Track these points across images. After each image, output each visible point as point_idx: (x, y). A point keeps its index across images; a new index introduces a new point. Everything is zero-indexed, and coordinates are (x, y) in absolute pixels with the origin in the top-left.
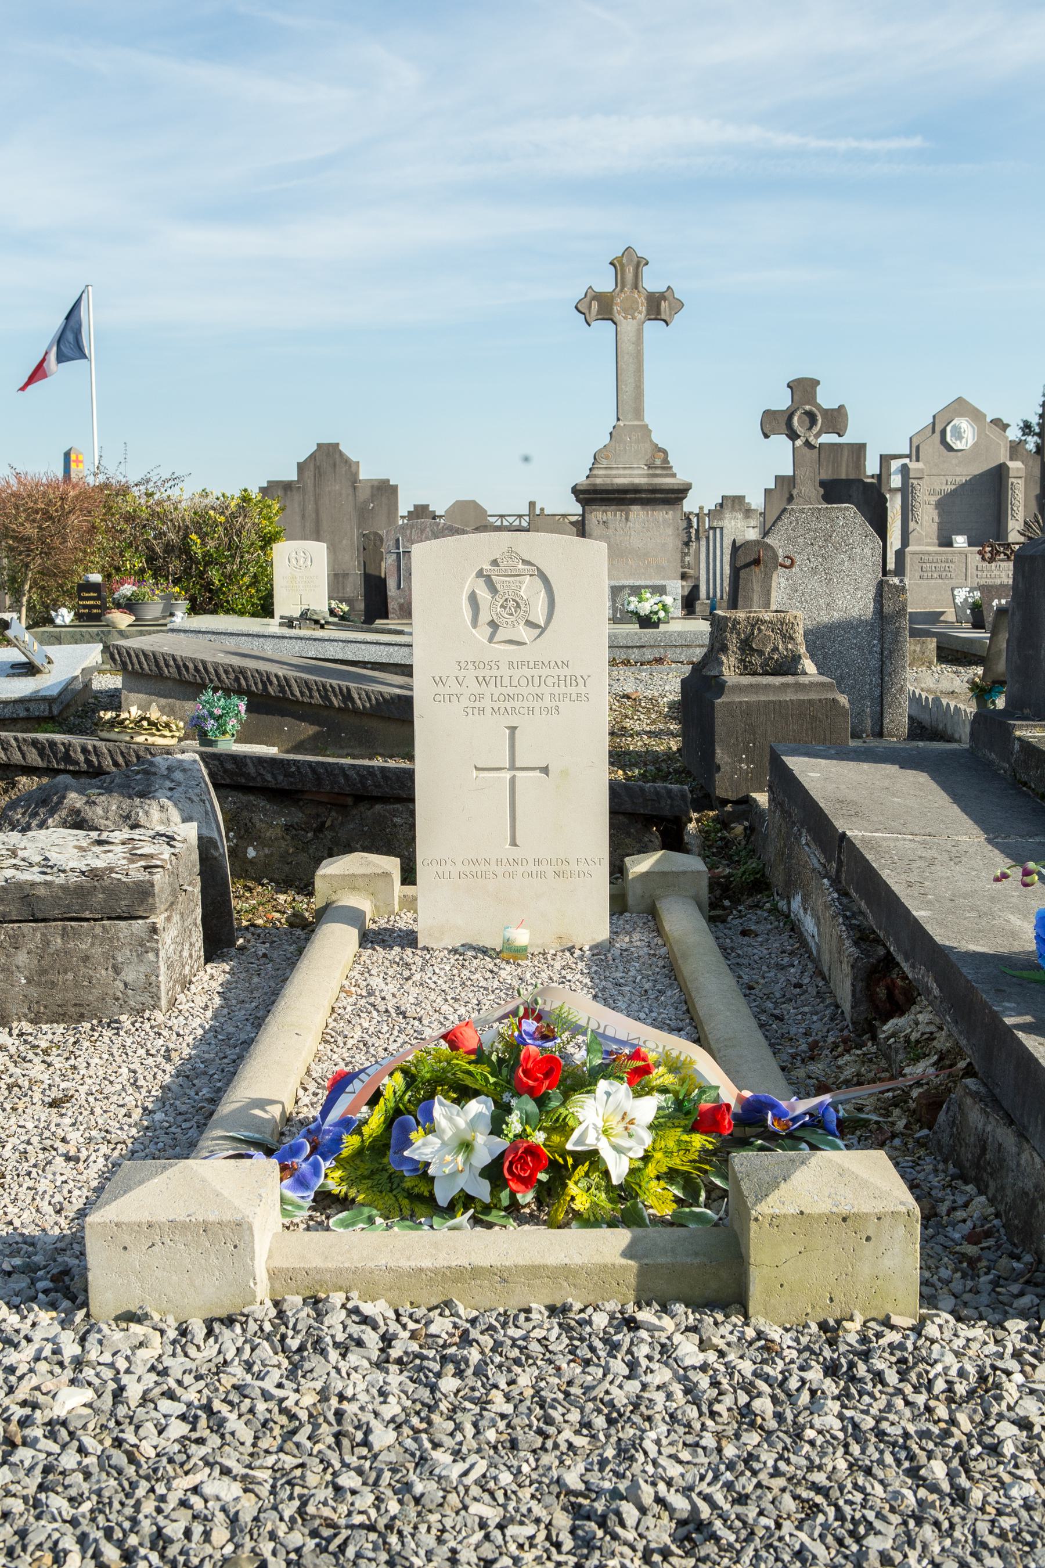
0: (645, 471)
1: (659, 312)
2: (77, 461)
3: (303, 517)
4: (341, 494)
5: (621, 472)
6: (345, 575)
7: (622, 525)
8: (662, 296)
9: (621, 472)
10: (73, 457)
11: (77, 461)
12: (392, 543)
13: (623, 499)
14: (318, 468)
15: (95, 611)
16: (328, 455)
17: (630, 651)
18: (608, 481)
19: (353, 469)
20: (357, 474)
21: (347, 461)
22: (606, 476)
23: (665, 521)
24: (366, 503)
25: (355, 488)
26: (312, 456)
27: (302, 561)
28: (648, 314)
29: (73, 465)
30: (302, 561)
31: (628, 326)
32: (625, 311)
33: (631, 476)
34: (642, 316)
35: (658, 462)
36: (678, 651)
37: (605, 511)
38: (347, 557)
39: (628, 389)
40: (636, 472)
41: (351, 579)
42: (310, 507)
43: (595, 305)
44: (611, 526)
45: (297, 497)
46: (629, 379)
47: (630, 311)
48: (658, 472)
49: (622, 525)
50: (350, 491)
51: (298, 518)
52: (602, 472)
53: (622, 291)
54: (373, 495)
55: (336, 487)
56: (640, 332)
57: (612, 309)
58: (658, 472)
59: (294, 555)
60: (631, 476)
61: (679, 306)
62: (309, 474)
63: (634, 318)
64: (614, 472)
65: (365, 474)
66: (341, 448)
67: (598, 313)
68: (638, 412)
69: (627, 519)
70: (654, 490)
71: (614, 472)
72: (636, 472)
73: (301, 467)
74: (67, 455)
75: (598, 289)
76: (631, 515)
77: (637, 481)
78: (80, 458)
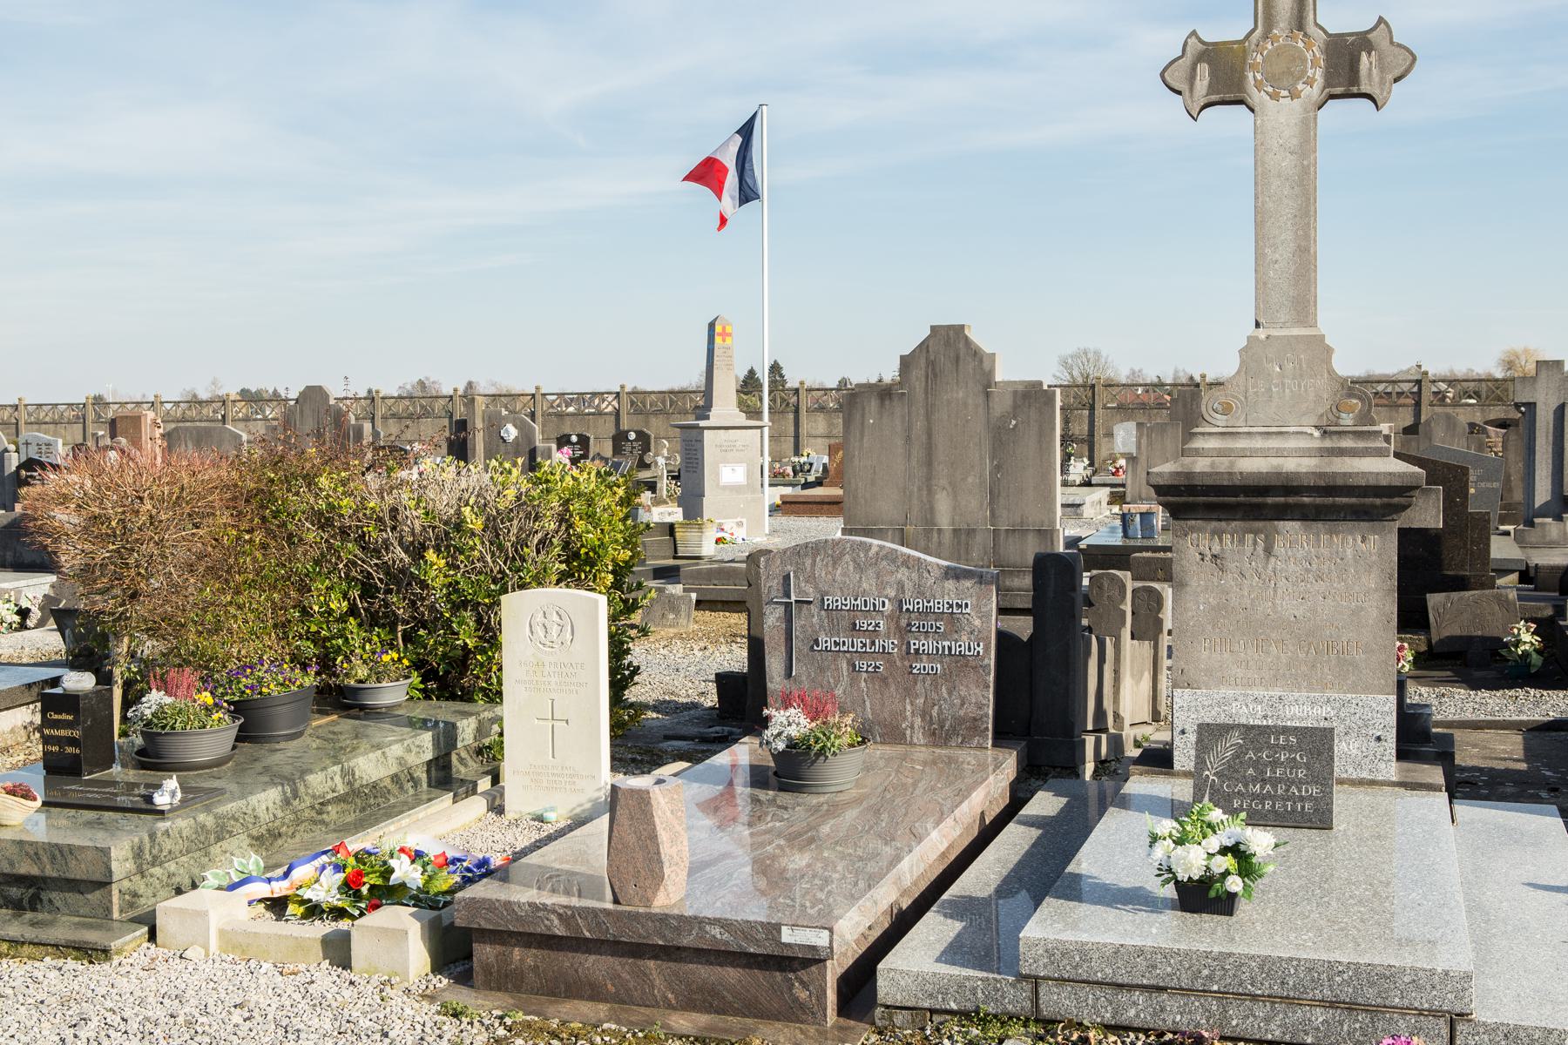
0: (1316, 442)
1: (1354, 78)
2: (724, 334)
3: (908, 439)
4: (965, 405)
5: (1259, 443)
6: (971, 532)
7: (1257, 564)
8: (1363, 42)
9: (1259, 443)
10: (718, 329)
11: (724, 334)
12: (775, 584)
13: (1259, 506)
14: (931, 364)
15: (69, 750)
16: (947, 344)
17: (1123, 997)
18: (1223, 465)
19: (986, 365)
20: (991, 372)
21: (976, 353)
22: (1221, 453)
23: (1358, 556)
24: (1004, 418)
25: (988, 395)
26: (924, 346)
27: (555, 630)
28: (1328, 83)
29: (718, 340)
30: (555, 630)
31: (1282, 113)
32: (1273, 79)
33: (1279, 453)
34: (1314, 92)
35: (1347, 420)
36: (1261, 1011)
37: (1219, 533)
38: (974, 504)
39: (1283, 254)
40: (1292, 443)
41: (979, 538)
42: (919, 425)
43: (1203, 70)
44: (1231, 566)
45: (898, 409)
46: (1285, 238)
47: (1283, 81)
48: (1347, 443)
49: (1257, 564)
50: (981, 400)
51: (900, 442)
52: (1212, 444)
53: (1265, 36)
54: (1015, 407)
55: (959, 394)
56: (1307, 129)
57: (1243, 78)
58: (1347, 443)
59: (539, 618)
60: (1279, 453)
61: (1405, 65)
62: (918, 374)
63: (1294, 95)
64: (1241, 444)
65: (1004, 373)
66: (973, 335)
67: (1212, 89)
68: (1304, 308)
69: (1268, 551)
70: (1330, 490)
71: (1241, 444)
72: (1292, 443)
73: (906, 363)
74: (712, 326)
75: (1211, 35)
76: (1279, 548)
77: (1291, 465)
78: (728, 329)
